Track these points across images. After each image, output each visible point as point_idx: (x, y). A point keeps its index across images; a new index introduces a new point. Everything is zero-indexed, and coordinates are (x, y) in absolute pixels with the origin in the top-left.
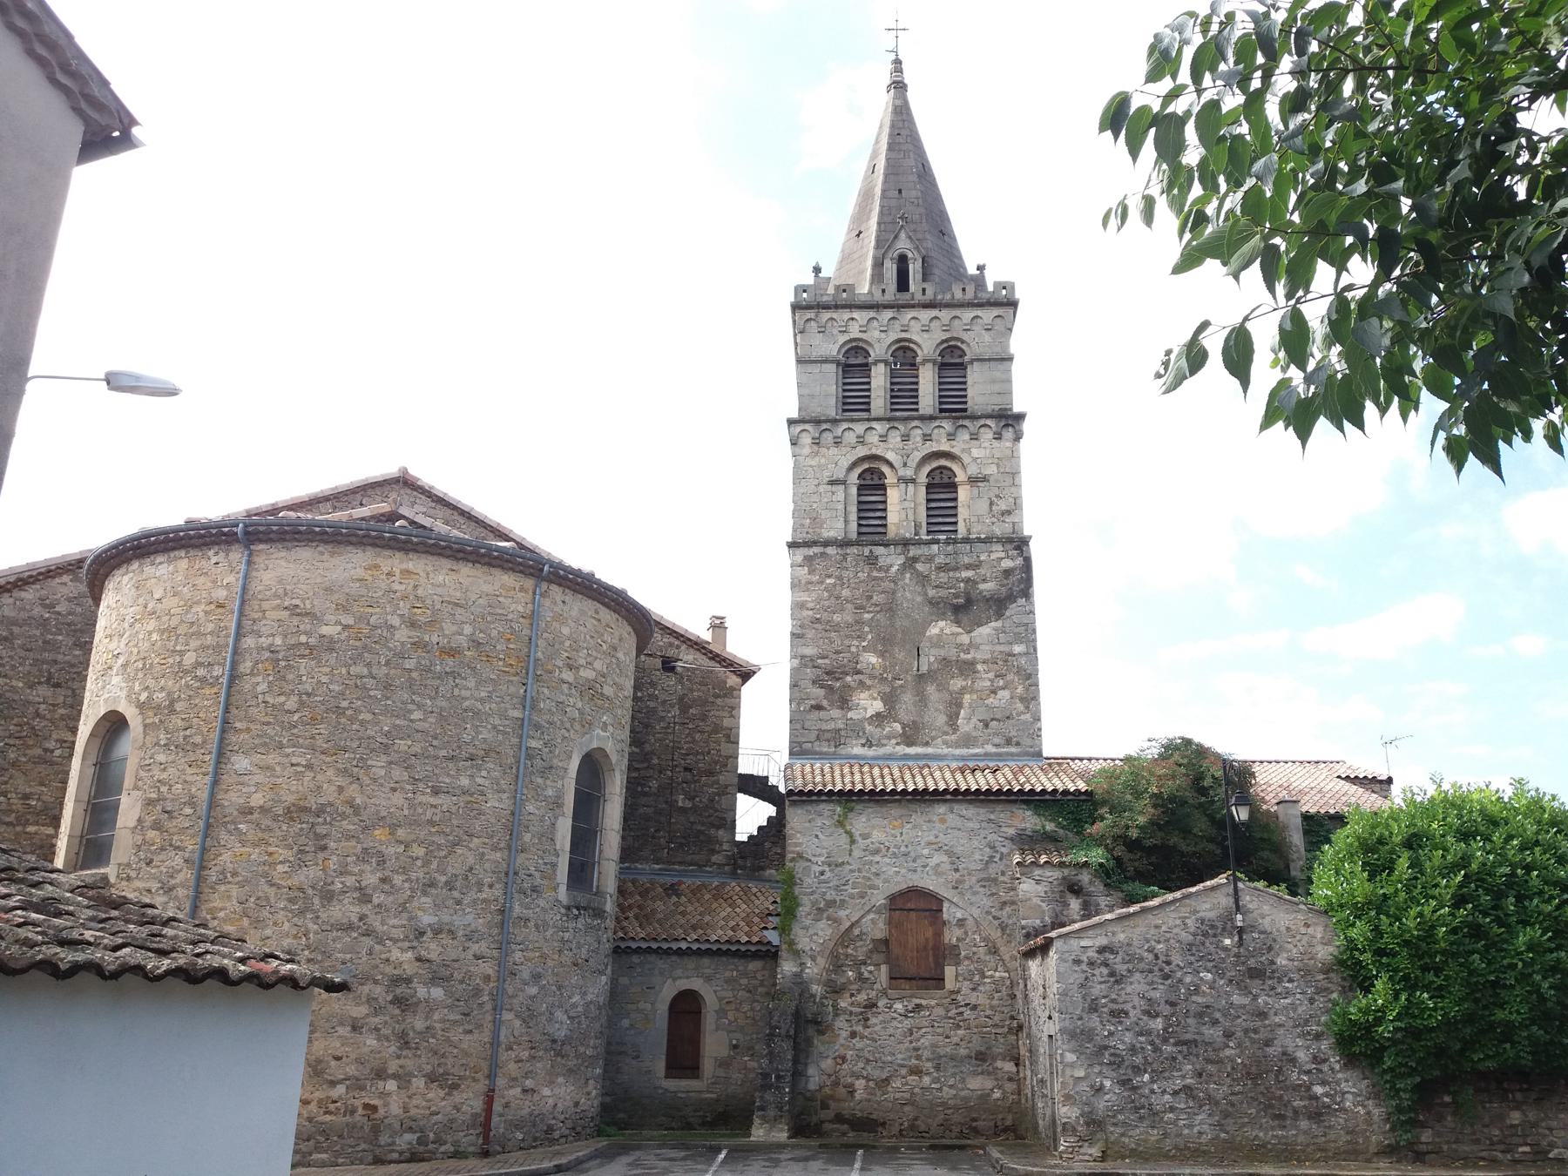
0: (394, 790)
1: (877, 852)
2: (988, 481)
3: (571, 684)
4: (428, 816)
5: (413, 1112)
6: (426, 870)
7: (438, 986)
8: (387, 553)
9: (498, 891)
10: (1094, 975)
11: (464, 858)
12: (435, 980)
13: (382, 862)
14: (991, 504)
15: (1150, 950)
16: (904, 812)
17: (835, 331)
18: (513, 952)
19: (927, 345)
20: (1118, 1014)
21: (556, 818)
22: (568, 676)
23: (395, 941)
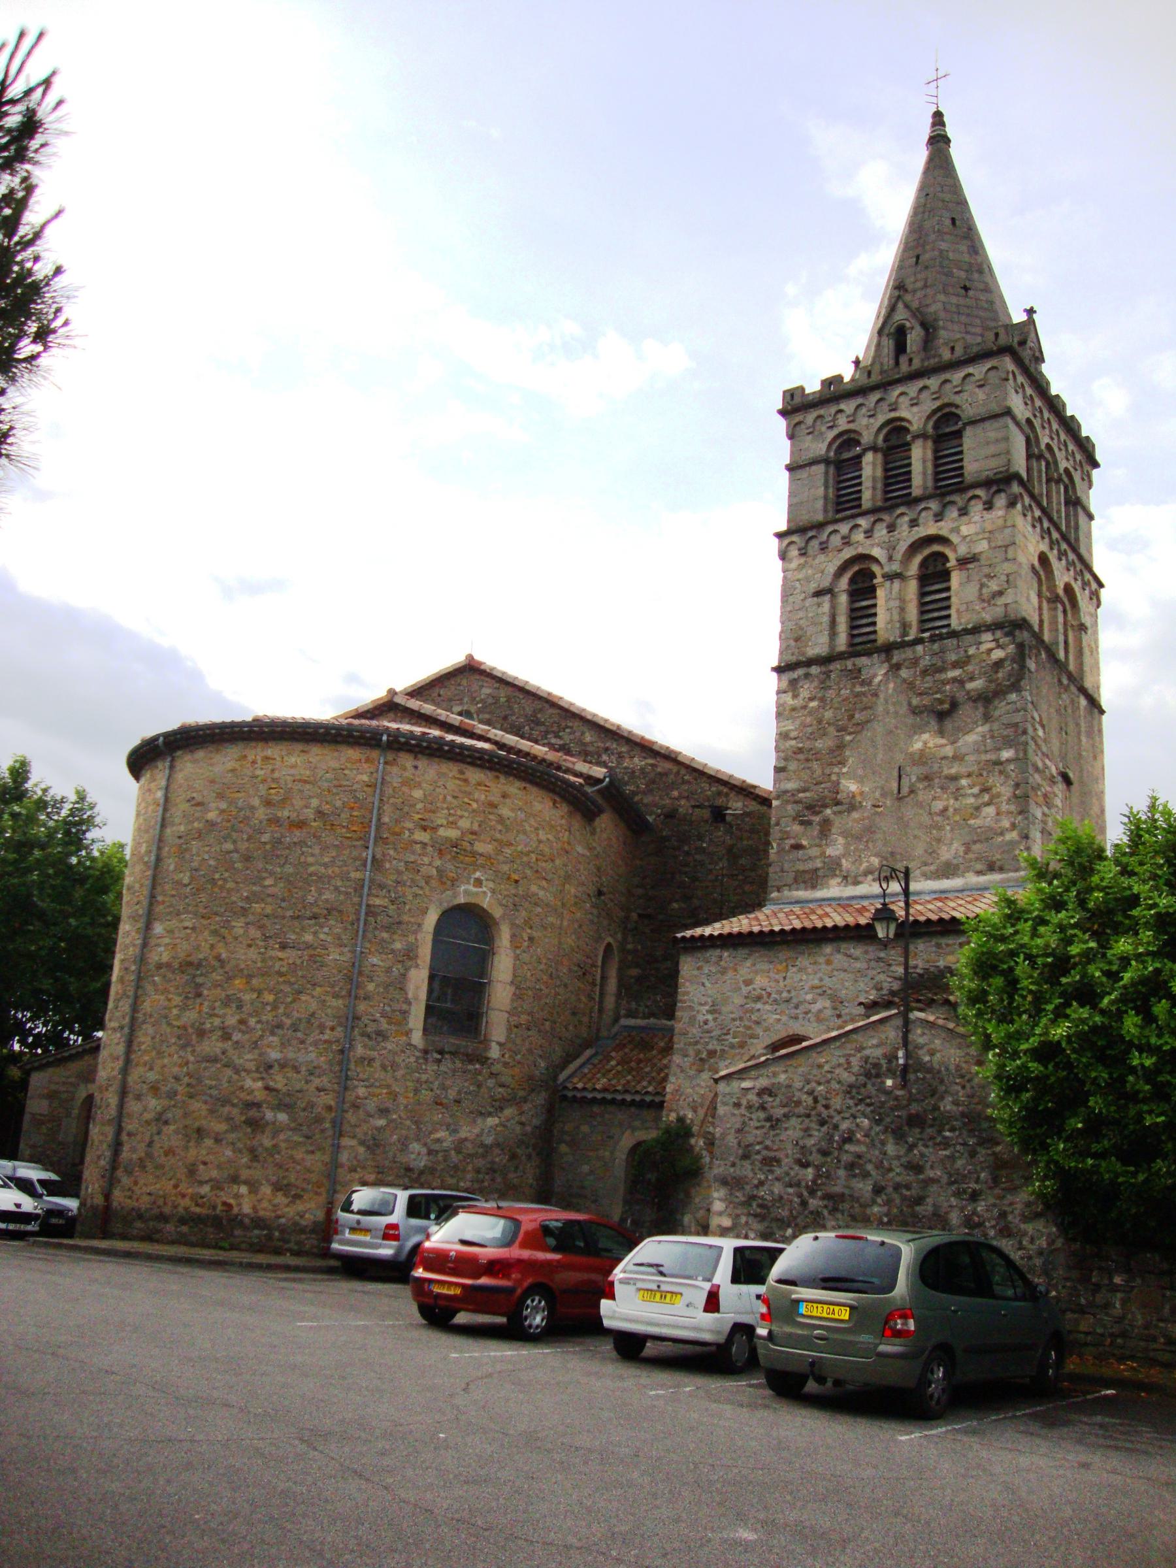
0: (250, 946)
1: (759, 998)
2: (978, 560)
3: (426, 844)
4: (277, 968)
5: (261, 1213)
6: (274, 1013)
7: (284, 1111)
8: (253, 744)
9: (339, 1032)
10: (751, 1119)
11: (308, 1003)
12: (282, 1106)
13: (240, 1007)
14: (982, 586)
15: (811, 1093)
16: (791, 954)
17: (824, 429)
18: (356, 1087)
19: (915, 416)
20: (770, 1162)
21: (407, 969)
22: (420, 836)
23: (248, 1072)
